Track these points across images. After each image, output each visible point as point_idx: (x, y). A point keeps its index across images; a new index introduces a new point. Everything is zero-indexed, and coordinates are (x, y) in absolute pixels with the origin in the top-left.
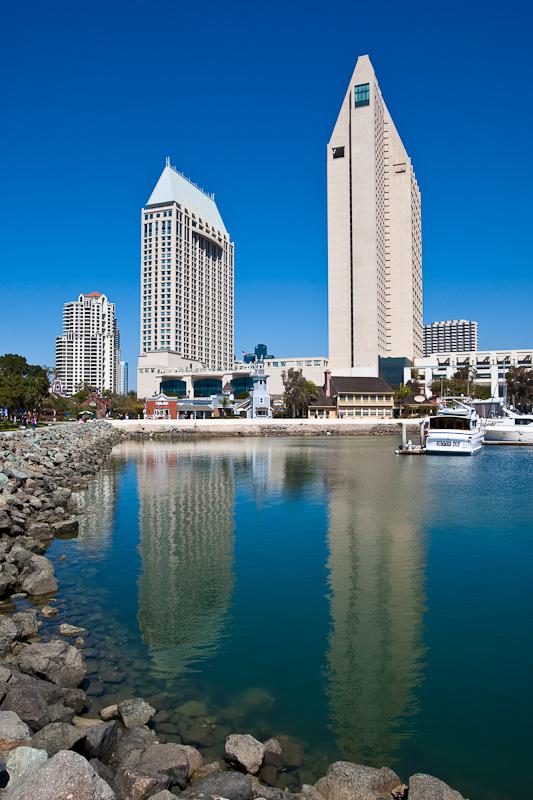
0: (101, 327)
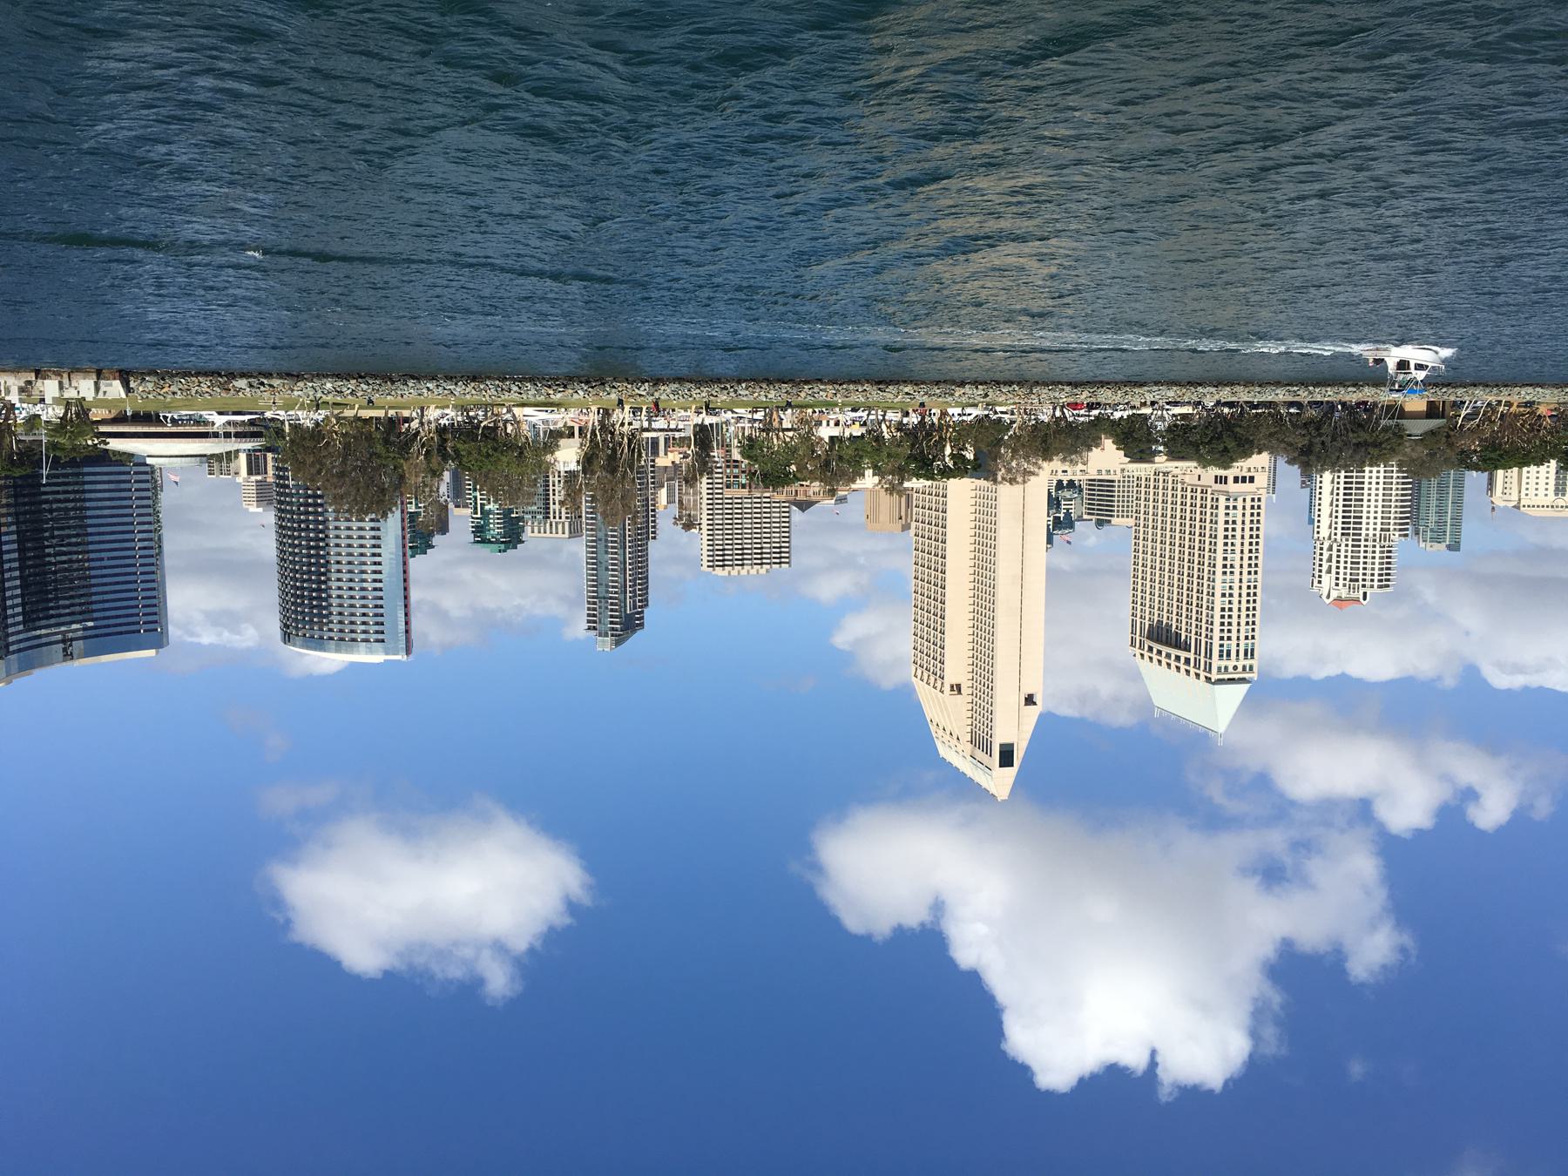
0: (1334, 553)
